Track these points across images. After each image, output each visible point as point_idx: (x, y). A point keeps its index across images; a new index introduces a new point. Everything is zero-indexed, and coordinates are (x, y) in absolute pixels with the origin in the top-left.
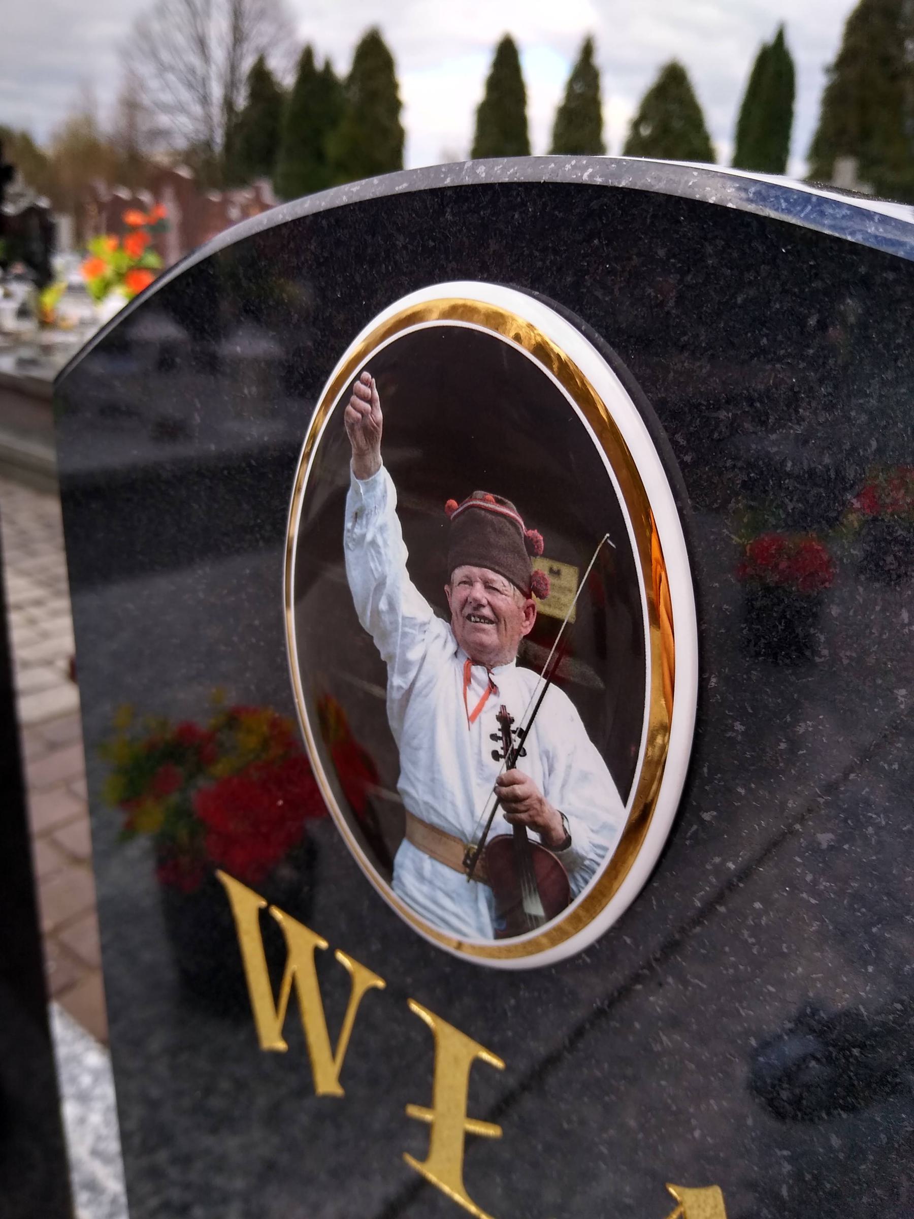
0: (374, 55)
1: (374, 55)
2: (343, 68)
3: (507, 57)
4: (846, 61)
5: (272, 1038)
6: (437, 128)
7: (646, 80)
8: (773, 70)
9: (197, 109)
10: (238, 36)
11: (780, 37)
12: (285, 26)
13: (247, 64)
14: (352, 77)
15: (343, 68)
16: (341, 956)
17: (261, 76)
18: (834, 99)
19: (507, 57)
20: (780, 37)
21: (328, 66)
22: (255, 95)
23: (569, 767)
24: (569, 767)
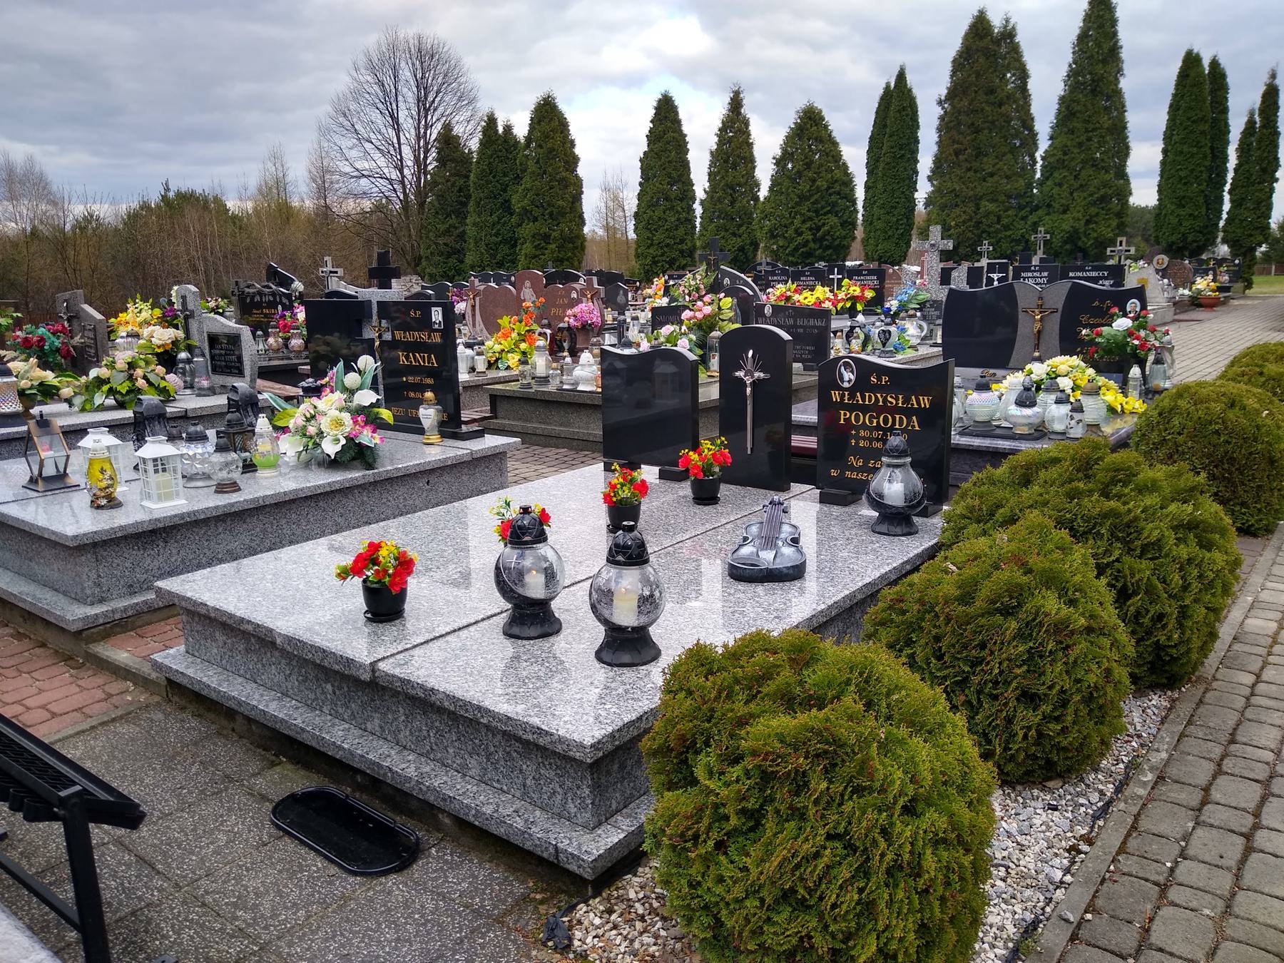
0: (548, 116)
1: (548, 116)
2: (521, 130)
3: (666, 112)
4: (954, 94)
5: (1071, 274)
6: (608, 164)
7: (790, 119)
8: (896, 107)
9: (395, 175)
10: (424, 108)
11: (901, 76)
12: (466, 99)
13: (434, 133)
14: (529, 139)
15: (521, 130)
16: (1144, 194)
17: (448, 141)
18: (947, 126)
19: (666, 112)
20: (901, 76)
21: (508, 129)
22: (441, 160)
23: (474, 325)
24: (474, 325)
